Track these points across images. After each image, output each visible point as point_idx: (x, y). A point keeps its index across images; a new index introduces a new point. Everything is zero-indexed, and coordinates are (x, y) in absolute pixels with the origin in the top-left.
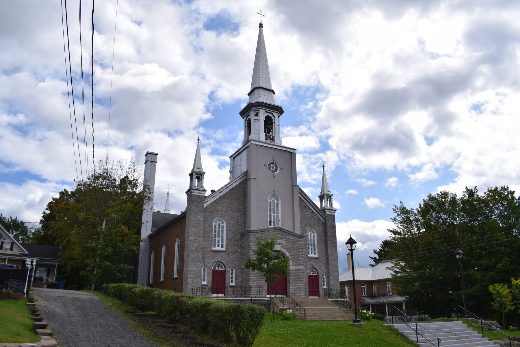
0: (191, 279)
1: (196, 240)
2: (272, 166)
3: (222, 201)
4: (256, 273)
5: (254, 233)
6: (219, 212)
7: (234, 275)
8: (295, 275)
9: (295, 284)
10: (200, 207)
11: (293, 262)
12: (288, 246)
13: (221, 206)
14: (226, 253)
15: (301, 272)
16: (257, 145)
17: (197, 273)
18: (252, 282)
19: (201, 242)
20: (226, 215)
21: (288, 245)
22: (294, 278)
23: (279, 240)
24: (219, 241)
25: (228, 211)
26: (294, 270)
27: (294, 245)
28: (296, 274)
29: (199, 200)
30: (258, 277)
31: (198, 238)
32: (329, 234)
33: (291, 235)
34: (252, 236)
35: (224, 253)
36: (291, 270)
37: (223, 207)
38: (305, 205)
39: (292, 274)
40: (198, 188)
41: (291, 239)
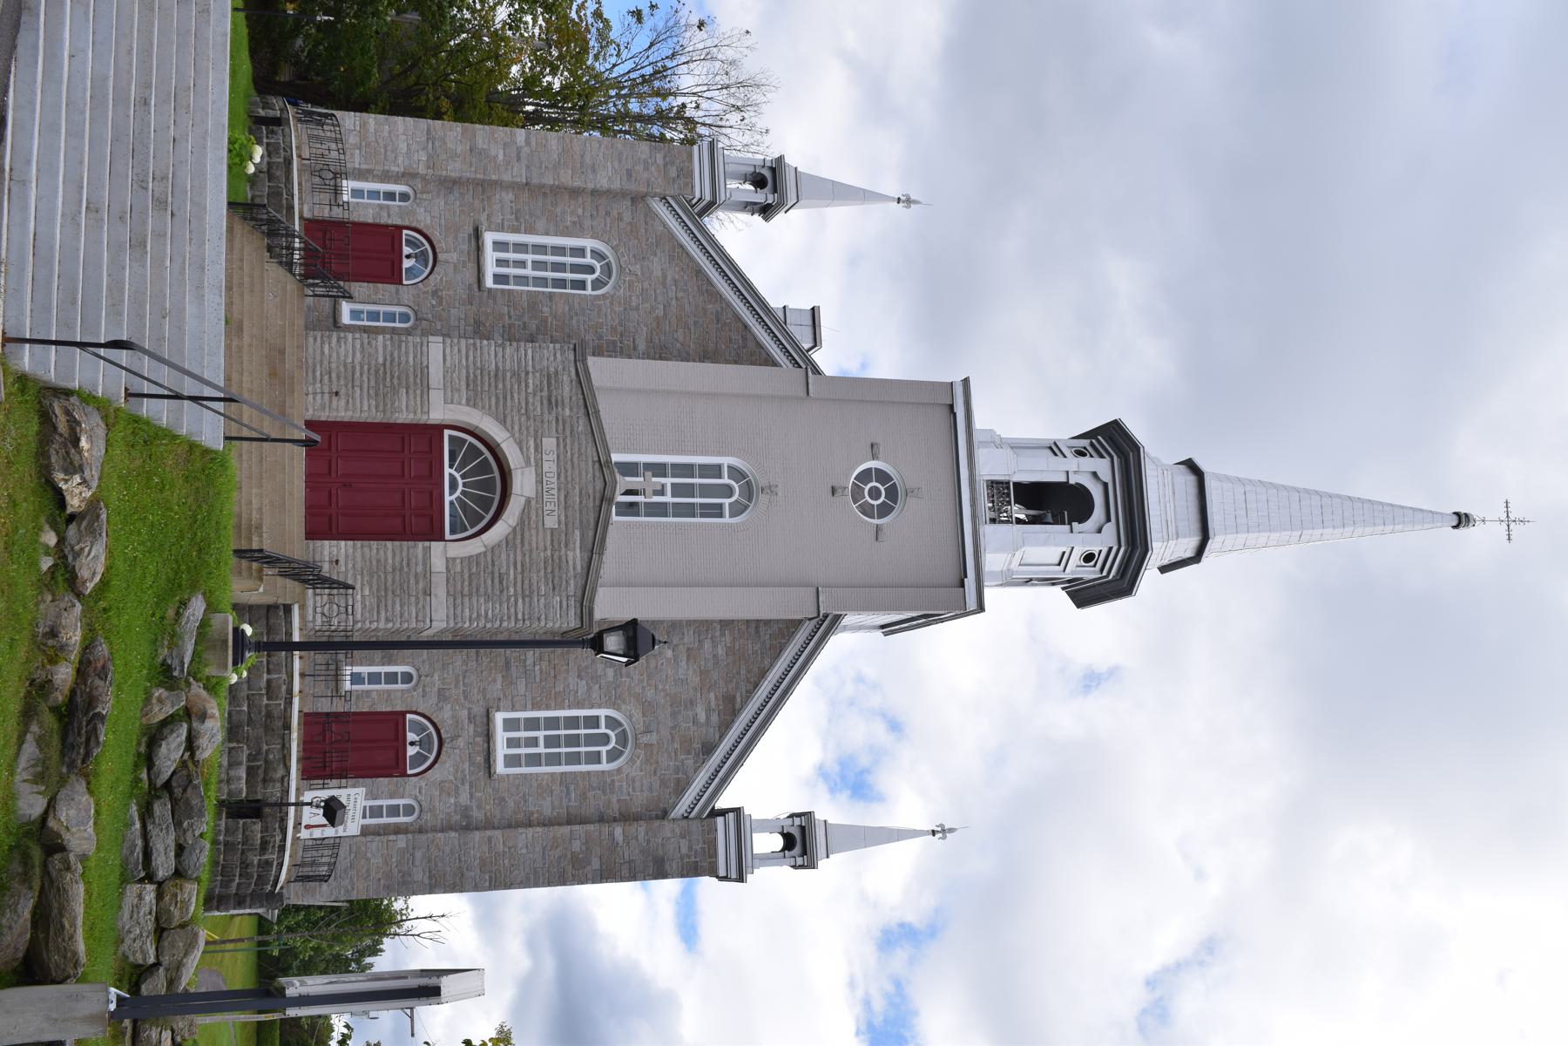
0: (358, 123)
1: (514, 155)
2: (877, 498)
3: (686, 278)
4: (399, 364)
5: (572, 364)
6: (638, 266)
7: (382, 309)
8: (401, 569)
9: (358, 566)
10: (646, 175)
11: (462, 559)
12: (534, 539)
13: (665, 276)
14: (476, 290)
15: (417, 604)
16: (951, 407)
17: (386, 151)
18: (362, 344)
19: (510, 172)
20: (630, 297)
21: (540, 537)
22: (390, 561)
23: (559, 489)
24: (522, 264)
25: (648, 305)
26: (425, 564)
27: (542, 573)
28: (408, 574)
29: (673, 172)
30: (385, 373)
31: (524, 162)
32: (618, 831)
33: (586, 555)
34: (558, 355)
35: (473, 280)
36: (427, 550)
37: (664, 283)
38: (739, 700)
39: (404, 554)
40: (721, 158)
41: (570, 554)
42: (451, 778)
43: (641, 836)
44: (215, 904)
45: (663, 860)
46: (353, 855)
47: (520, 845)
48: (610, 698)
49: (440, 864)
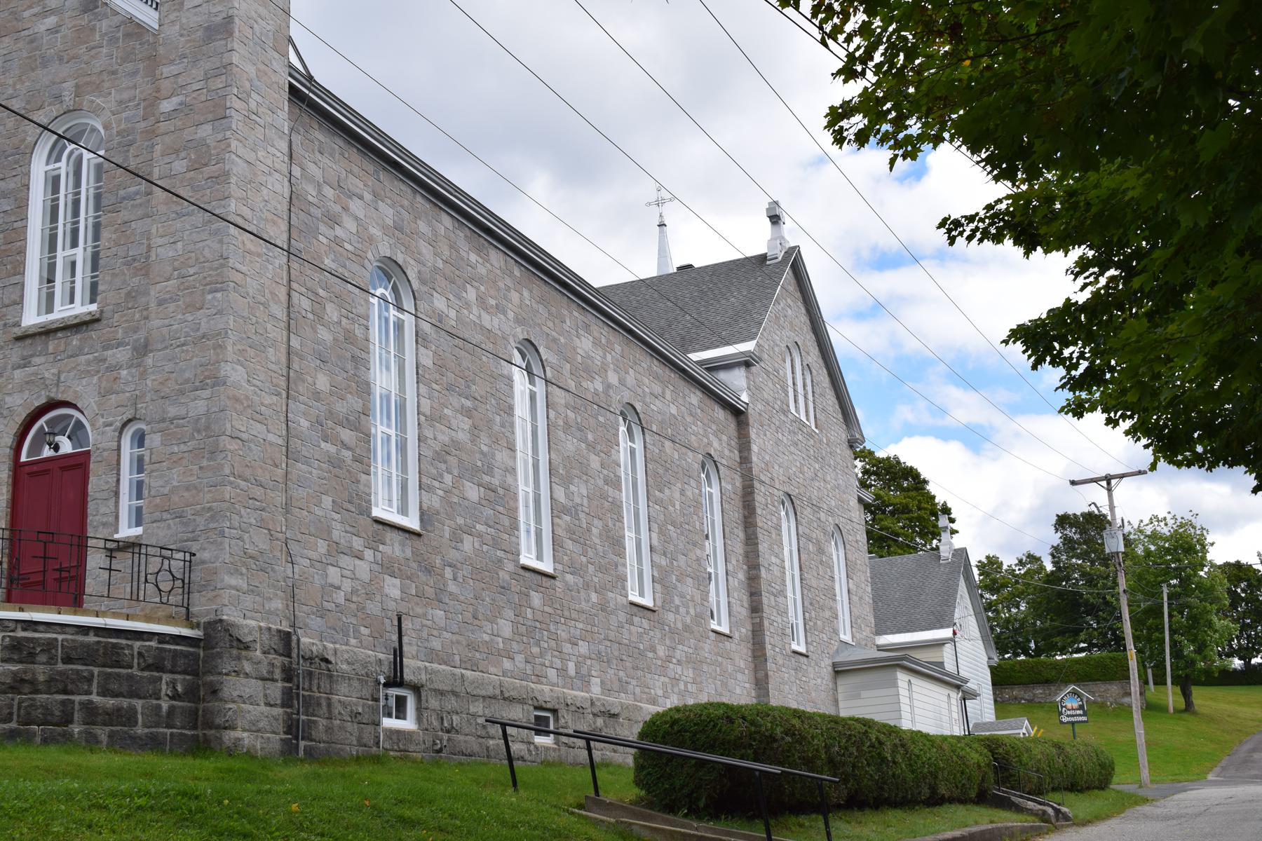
42: (95, 379)
43: (174, 69)
44: (213, 732)
45: (208, 29)
46: (165, 516)
47: (171, 254)
48: (16, 162)
49: (187, 375)
